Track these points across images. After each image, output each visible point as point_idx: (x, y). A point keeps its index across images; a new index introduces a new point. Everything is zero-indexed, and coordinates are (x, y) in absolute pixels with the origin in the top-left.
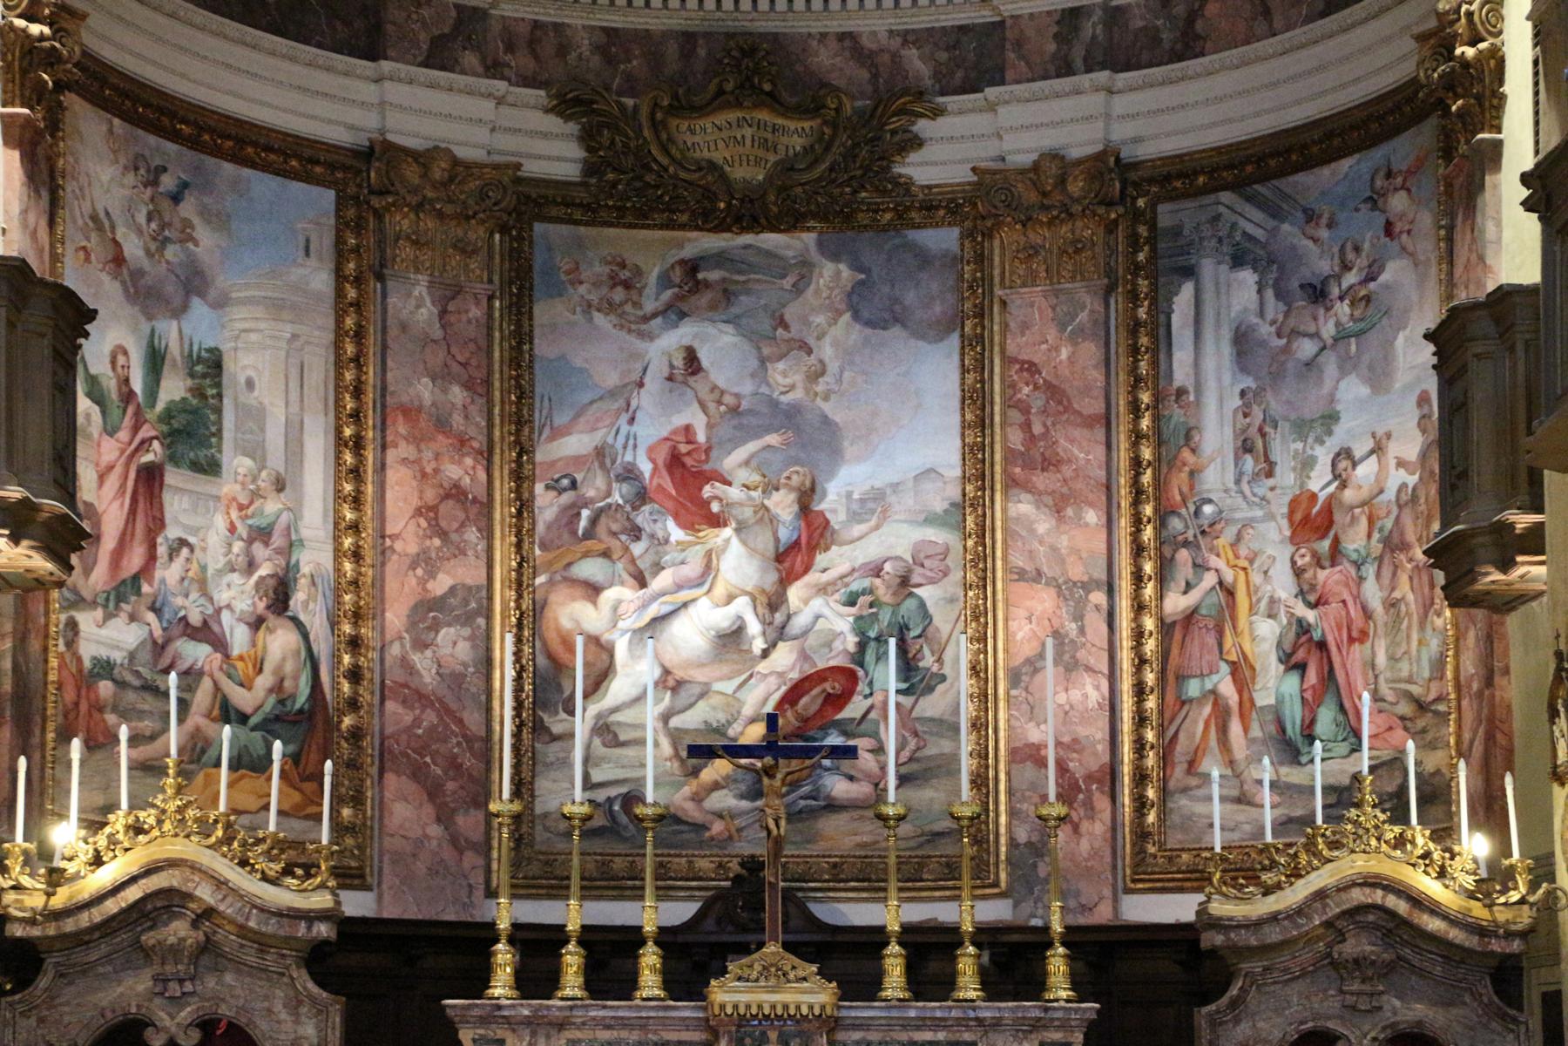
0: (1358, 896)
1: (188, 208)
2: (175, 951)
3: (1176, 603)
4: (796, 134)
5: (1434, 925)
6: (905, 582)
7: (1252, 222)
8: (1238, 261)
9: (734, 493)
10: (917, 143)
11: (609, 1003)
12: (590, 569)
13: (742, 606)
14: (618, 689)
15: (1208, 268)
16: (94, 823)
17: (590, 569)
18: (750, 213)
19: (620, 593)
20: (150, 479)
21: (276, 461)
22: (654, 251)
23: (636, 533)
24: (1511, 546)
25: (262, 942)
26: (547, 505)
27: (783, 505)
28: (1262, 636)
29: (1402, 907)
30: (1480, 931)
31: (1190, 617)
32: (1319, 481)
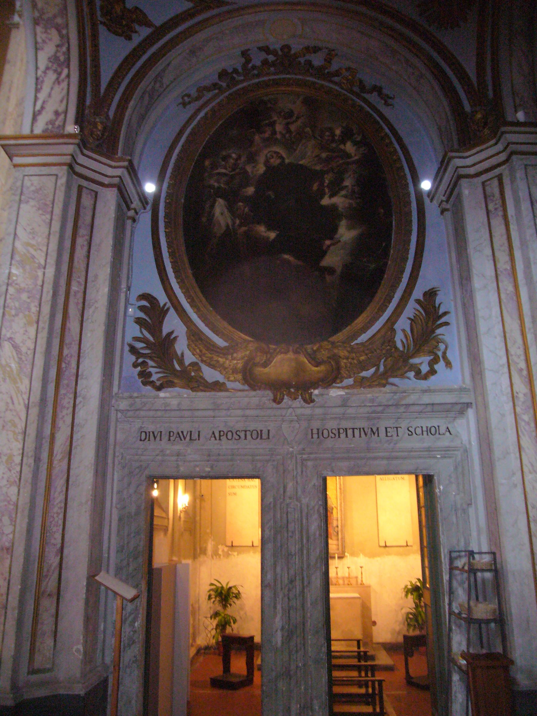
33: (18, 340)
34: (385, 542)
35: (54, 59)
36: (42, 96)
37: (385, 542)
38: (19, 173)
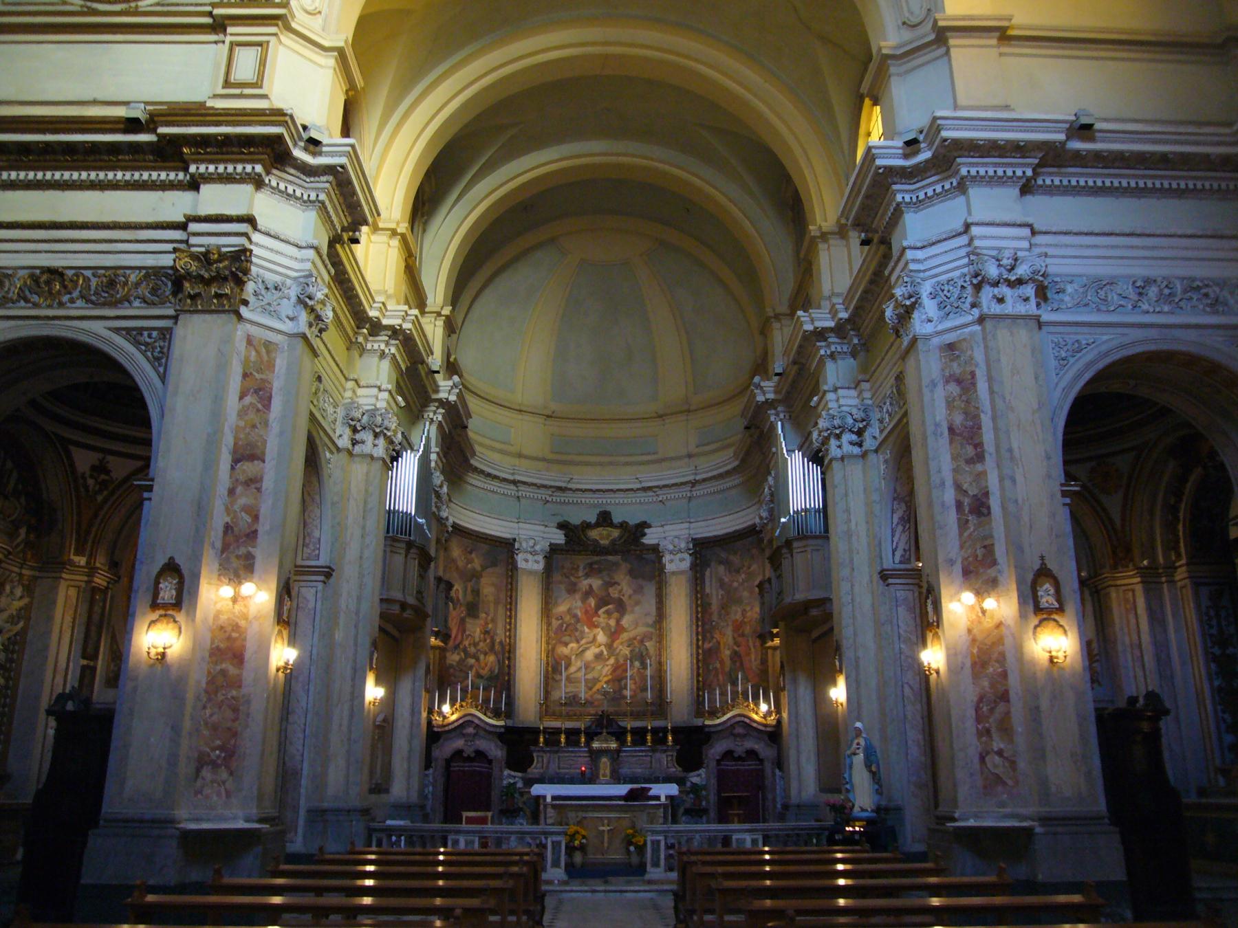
0: (738, 719)
1: (473, 555)
2: (469, 735)
3: (707, 646)
4: (616, 533)
5: (755, 725)
6: (642, 641)
7: (723, 555)
8: (721, 563)
9: (601, 620)
10: (645, 534)
11: (645, 162)
12: (566, 639)
13: (603, 648)
14: (572, 669)
15: (713, 564)
16: (452, 705)
17: (566, 639)
18: (604, 551)
19: (573, 645)
20: (462, 621)
21: (491, 615)
22: (582, 561)
23: (576, 630)
24: (773, 636)
25: (490, 733)
26: (555, 623)
27: (612, 623)
28: (727, 653)
29: (747, 721)
30: (765, 726)
31: (710, 649)
32: (739, 617)
33: (911, 683)
34: (1042, 558)
35: (902, 519)
36: (896, 539)
37: (1042, 558)
38: (892, 588)
